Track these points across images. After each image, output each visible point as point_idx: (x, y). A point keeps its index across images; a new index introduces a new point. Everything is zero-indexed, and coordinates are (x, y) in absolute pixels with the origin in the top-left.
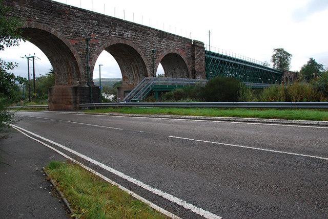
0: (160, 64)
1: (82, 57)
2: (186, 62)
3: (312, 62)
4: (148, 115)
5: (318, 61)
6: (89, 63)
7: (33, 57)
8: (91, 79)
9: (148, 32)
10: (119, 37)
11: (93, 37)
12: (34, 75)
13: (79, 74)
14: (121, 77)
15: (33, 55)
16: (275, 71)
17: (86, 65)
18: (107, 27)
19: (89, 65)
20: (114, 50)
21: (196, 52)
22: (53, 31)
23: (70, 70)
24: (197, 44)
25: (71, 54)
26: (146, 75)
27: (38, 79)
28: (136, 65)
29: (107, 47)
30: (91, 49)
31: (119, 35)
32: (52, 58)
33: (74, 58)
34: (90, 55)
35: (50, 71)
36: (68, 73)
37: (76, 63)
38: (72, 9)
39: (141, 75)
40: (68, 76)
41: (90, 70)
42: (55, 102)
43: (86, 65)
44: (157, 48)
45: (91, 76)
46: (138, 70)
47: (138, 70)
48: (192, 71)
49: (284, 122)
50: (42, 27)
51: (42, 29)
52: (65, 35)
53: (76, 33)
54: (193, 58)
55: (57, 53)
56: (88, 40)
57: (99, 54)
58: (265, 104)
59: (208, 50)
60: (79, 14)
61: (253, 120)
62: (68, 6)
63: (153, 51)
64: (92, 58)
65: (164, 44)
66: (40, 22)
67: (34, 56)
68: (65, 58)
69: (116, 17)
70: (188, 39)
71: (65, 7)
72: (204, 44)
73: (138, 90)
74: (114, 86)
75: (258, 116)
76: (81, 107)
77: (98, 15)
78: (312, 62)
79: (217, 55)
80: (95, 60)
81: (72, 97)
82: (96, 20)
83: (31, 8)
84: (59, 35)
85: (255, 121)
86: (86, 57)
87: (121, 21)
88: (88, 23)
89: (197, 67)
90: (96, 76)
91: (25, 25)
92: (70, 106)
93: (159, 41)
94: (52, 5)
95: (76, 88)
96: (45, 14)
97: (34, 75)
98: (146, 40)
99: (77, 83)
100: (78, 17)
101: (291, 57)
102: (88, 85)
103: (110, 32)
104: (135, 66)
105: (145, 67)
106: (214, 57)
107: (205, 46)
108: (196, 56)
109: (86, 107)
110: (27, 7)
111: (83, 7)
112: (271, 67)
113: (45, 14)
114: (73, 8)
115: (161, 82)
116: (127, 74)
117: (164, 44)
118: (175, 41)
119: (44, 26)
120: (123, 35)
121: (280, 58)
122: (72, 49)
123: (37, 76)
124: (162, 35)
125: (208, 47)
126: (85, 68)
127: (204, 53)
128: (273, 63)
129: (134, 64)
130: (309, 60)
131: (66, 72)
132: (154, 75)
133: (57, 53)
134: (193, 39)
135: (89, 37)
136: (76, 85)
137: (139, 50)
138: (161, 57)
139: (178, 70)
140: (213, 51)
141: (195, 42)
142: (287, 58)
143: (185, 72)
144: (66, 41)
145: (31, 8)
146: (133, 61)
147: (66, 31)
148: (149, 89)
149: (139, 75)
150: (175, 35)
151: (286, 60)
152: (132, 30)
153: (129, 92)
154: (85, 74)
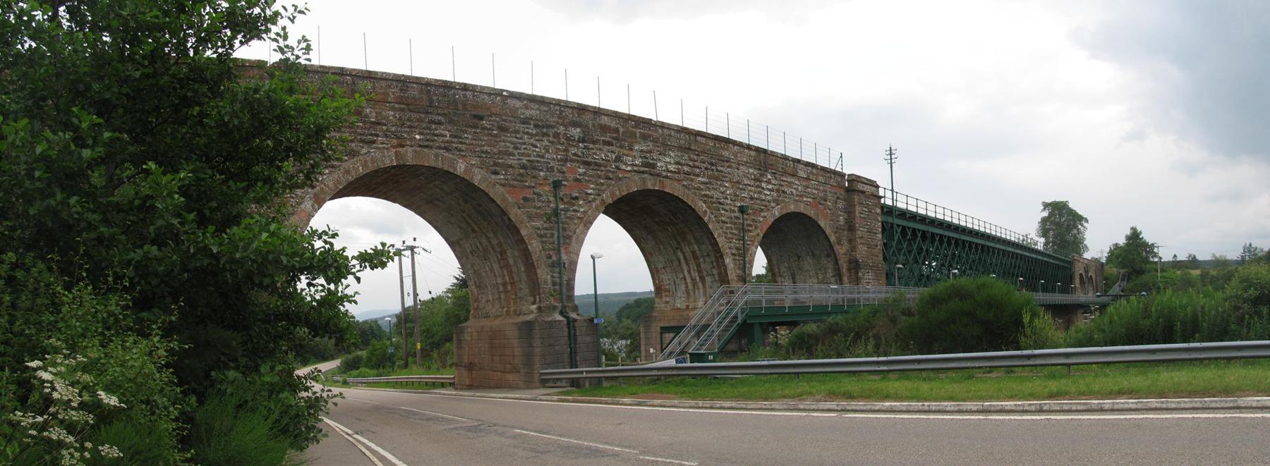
0: (759, 248)
1: (541, 236)
2: (833, 239)
3: (1135, 236)
4: (934, 405)
5: (1148, 237)
6: (562, 250)
7: (412, 248)
8: (571, 297)
9: (726, 153)
10: (643, 172)
11: (570, 176)
12: (416, 295)
13: (535, 287)
15: (410, 243)
16: (1049, 256)
17: (554, 258)
18: (610, 144)
19: (564, 257)
20: (625, 211)
21: (858, 209)
22: (460, 168)
23: (510, 272)
24: (860, 187)
25: (513, 229)
26: (724, 279)
27: (423, 303)
28: (693, 253)
29: (610, 201)
30: (566, 210)
32: (460, 246)
33: (521, 240)
34: (564, 229)
35: (456, 281)
36: (504, 284)
37: (526, 255)
38: (509, 101)
39: (708, 279)
40: (506, 291)
41: (566, 270)
43: (554, 258)
44: (752, 198)
45: (570, 286)
46: (698, 266)
47: (698, 266)
48: (850, 262)
50: (431, 159)
51: (433, 164)
52: (493, 177)
53: (524, 167)
54: (851, 227)
55: (474, 231)
56: (557, 185)
58: (919, 361)
59: (889, 202)
60: (528, 113)
61: (1183, 405)
62: (498, 93)
63: (742, 210)
64: (570, 237)
65: (770, 187)
66: (426, 147)
68: (494, 242)
69: (633, 113)
70: (835, 172)
71: (490, 94)
72: (878, 187)
75: (1130, 393)
76: (547, 381)
77: (582, 109)
78: (1135, 236)
79: (914, 217)
80: (580, 242)
81: (518, 351)
82: (575, 124)
83: (402, 110)
84: (478, 177)
85: (1126, 406)
86: (552, 235)
88: (557, 135)
89: (861, 252)
90: (582, 287)
91: (387, 158)
92: (510, 377)
95: (529, 325)
96: (440, 123)
97: (416, 295)
99: (531, 311)
100: (525, 121)
101: (1085, 224)
103: (618, 159)
104: (689, 255)
105: (719, 255)
106: (905, 223)
107: (881, 193)
108: (858, 221)
109: (561, 380)
110: (393, 109)
111: (539, 92)
112: (1040, 247)
113: (440, 123)
114: (513, 95)
115: (762, 296)
116: (666, 277)
117: (770, 187)
118: (799, 178)
119: (437, 156)
120: (653, 166)
121: (1059, 225)
122: (515, 214)
123: (424, 296)
124: (764, 160)
125: (889, 194)
126: (553, 265)
127: (879, 211)
129: (687, 249)
130: (1128, 232)
131: (500, 280)
132: (744, 277)
133: (474, 231)
135: (559, 177)
136: (530, 317)
137: (701, 206)
138: (760, 232)
139: (808, 263)
140: (901, 205)
141: (855, 179)
142: (1075, 227)
143: (830, 266)
144: (497, 193)
146: (684, 239)
147: (496, 164)
148: (736, 317)
149: (702, 279)
150: (799, 161)
152: (681, 149)
153: (677, 330)
154: (554, 284)
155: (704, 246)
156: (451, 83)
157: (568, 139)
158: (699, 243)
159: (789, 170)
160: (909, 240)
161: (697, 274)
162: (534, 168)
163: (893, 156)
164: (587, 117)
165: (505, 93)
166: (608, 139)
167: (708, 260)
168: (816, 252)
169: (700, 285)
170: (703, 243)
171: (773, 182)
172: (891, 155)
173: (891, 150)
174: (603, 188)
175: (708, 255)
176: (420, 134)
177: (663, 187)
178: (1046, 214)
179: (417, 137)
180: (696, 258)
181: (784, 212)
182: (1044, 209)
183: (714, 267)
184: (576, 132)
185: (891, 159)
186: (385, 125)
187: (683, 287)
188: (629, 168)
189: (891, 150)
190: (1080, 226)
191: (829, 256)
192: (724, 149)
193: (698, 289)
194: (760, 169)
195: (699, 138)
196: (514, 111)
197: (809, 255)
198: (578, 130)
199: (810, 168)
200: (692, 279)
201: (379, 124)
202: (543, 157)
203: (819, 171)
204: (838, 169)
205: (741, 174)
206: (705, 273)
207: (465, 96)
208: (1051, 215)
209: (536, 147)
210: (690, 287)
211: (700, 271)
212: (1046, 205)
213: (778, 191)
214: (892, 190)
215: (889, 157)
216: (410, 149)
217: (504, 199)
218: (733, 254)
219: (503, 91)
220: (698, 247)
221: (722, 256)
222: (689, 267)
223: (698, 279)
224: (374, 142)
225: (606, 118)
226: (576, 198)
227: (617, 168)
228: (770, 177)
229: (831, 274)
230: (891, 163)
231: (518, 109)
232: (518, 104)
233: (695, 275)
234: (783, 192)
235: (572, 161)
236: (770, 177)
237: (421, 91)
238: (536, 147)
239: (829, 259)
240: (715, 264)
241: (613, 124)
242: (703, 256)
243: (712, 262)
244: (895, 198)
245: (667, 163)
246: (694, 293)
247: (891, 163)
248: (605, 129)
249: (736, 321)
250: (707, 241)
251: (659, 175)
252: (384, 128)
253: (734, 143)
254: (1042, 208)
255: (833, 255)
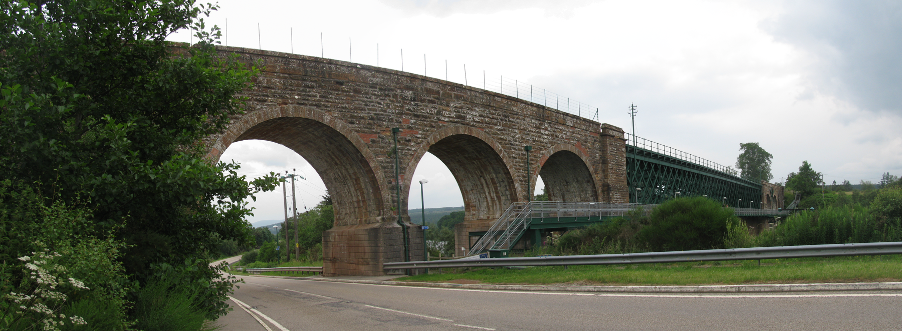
0: (539, 178)
2: (591, 169)
3: (806, 168)
4: (663, 287)
5: (815, 168)
6: (399, 178)
7: (292, 176)
8: (405, 211)
10: (457, 122)
11: (405, 125)
12: (295, 209)
13: (380, 204)
14: (463, 205)
15: (291, 172)
16: (745, 182)
17: (394, 183)
19: (401, 182)
20: (444, 150)
21: (609, 148)
22: (327, 119)
23: (363, 193)
24: (611, 132)
25: (364, 162)
26: (514, 198)
28: (492, 179)
29: (433, 143)
30: (402, 149)
31: (459, 117)
32: (327, 175)
33: (370, 171)
34: (401, 163)
35: (323, 200)
36: (358, 202)
37: (374, 181)
38: (361, 71)
39: (503, 198)
40: (359, 207)
41: (402, 192)
42: (334, 260)
43: (394, 183)
44: (534, 141)
45: (405, 203)
46: (496, 189)
47: (496, 189)
48: (604, 186)
49: (862, 288)
50: (306, 113)
51: (307, 117)
52: (350, 125)
53: (372, 119)
54: (604, 161)
55: (336, 164)
56: (395, 131)
57: (418, 159)
58: (653, 257)
59: (631, 144)
60: (375, 80)
62: (354, 66)
63: (527, 149)
64: (404, 169)
65: (547, 132)
67: (295, 173)
68: (351, 172)
70: (593, 122)
71: (348, 67)
72: (623, 133)
73: (499, 229)
74: (440, 224)
75: (803, 279)
76: (388, 270)
77: (413, 77)
79: (649, 154)
81: (368, 249)
82: (408, 88)
83: (286, 78)
84: (339, 126)
85: (800, 288)
86: (392, 167)
87: (459, 87)
88: (395, 96)
89: (612, 179)
90: (414, 204)
91: (275, 113)
93: (537, 127)
94: (323, 67)
95: (375, 231)
96: (312, 87)
97: (295, 209)
98: (511, 126)
99: (377, 220)
100: (373, 86)
101: (771, 159)
102: (399, 222)
103: (439, 113)
104: (489, 181)
105: (511, 181)
107: (626, 137)
110: (279, 77)
111: (383, 65)
112: (739, 175)
113: (312, 87)
114: (364, 68)
115: (541, 210)
117: (547, 132)
118: (567, 126)
119: (310, 111)
120: (464, 118)
121: (752, 159)
122: (366, 152)
123: (301, 210)
124: (543, 113)
125: (631, 138)
126: (392, 188)
127: (624, 149)
128: (740, 170)
129: (488, 177)
130: (801, 165)
131: (355, 199)
132: (529, 197)
133: (336, 164)
134: (602, 121)
135: (397, 125)
136: (376, 225)
137: (498, 147)
138: (540, 165)
139: (574, 187)
141: (607, 127)
142: (764, 161)
144: (353, 137)
145: (286, 78)
147: (352, 117)
148: (522, 225)
149: (499, 198)
150: (567, 114)
151: (763, 164)
152: (483, 105)
153: (481, 234)
154: (393, 201)
155: (500, 175)
156: (320, 59)
157: (403, 98)
158: (496, 173)
159: (560, 121)
160: (645, 170)
161: (495, 195)
162: (379, 119)
163: (634, 111)
164: (417, 83)
165: (358, 66)
166: (432, 99)
167: (503, 184)
168: (579, 179)
169: (497, 202)
170: (499, 173)
171: (549, 129)
172: (633, 110)
173: (632, 107)
174: (428, 133)
175: (503, 181)
176: (298, 95)
177: (471, 133)
178: (743, 152)
179: (296, 97)
180: (494, 183)
181: (557, 150)
182: (742, 148)
183: (507, 190)
184: (409, 94)
185: (633, 113)
186: (273, 88)
187: (485, 203)
188: (447, 119)
189: (632, 107)
190: (767, 161)
191: (588, 182)
192: (514, 106)
193: (496, 205)
194: (540, 120)
195: (496, 98)
196: (365, 80)
197: (574, 181)
198: (411, 92)
199: (575, 119)
200: (491, 198)
201: (269, 88)
202: (385, 111)
203: (582, 121)
204: (595, 120)
205: (526, 124)
206: (500, 194)
207: (330, 68)
208: (746, 152)
209: (381, 104)
210: (490, 204)
211: (497, 193)
212: (743, 146)
213: (552, 135)
214: (634, 135)
215: (631, 111)
216: (291, 106)
217: (358, 141)
218: (521, 181)
219: (357, 64)
220: (496, 175)
221: (512, 182)
222: (489, 190)
223: (495, 198)
224: (265, 101)
225: (430, 84)
226: (409, 141)
227: (438, 119)
228: (546, 126)
229: (590, 195)
230: (633, 116)
231: (367, 77)
232: (368, 74)
233: (494, 195)
234: (556, 136)
235: (406, 114)
236: (546, 126)
237: (299, 65)
238: (381, 104)
239: (589, 184)
240: (508, 188)
241: (435, 88)
242: (499, 182)
243: (506, 186)
244: (635, 141)
245: (473, 115)
246: (493, 208)
247: (633, 116)
248: (429, 91)
249: (523, 228)
250: (502, 172)
251: (468, 124)
252: (273, 91)
253: (522, 101)
254: (740, 147)
255: (591, 181)
